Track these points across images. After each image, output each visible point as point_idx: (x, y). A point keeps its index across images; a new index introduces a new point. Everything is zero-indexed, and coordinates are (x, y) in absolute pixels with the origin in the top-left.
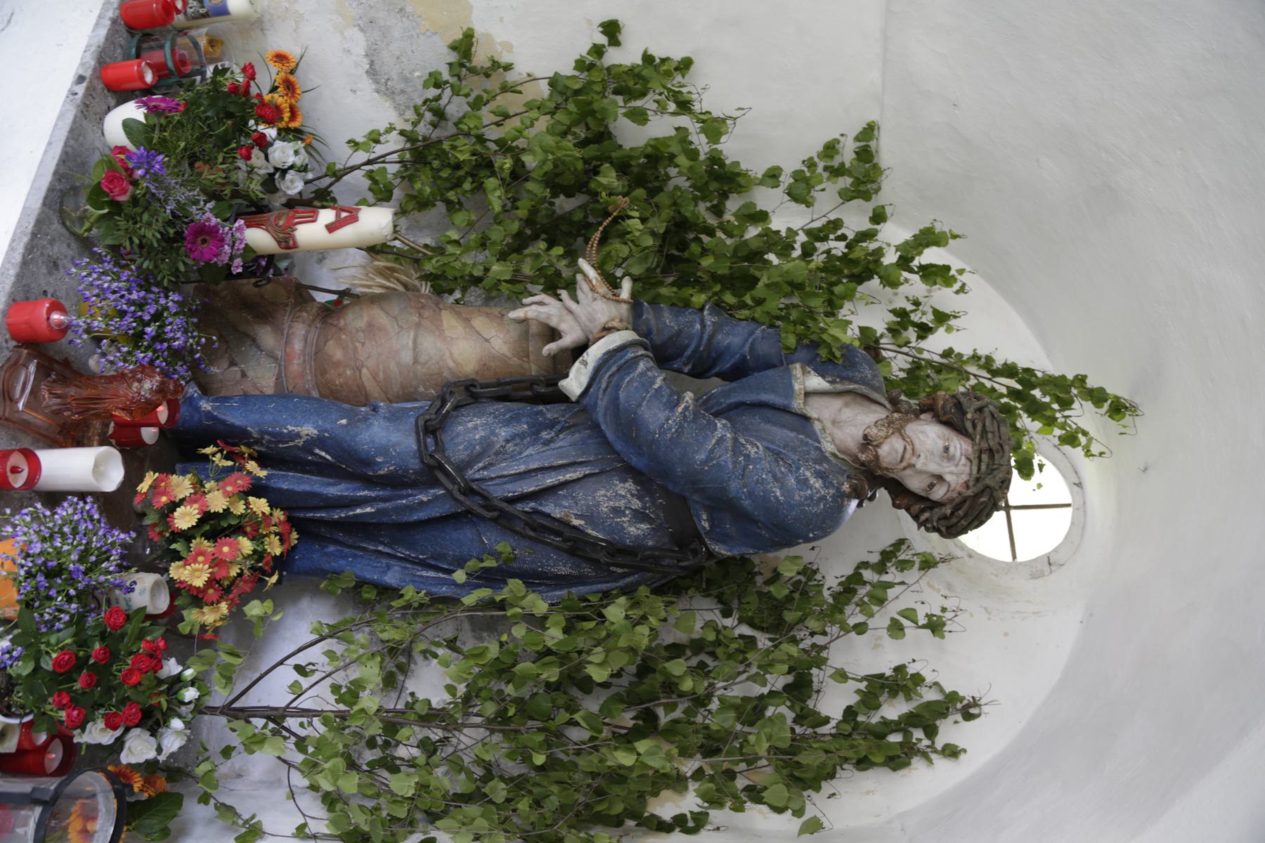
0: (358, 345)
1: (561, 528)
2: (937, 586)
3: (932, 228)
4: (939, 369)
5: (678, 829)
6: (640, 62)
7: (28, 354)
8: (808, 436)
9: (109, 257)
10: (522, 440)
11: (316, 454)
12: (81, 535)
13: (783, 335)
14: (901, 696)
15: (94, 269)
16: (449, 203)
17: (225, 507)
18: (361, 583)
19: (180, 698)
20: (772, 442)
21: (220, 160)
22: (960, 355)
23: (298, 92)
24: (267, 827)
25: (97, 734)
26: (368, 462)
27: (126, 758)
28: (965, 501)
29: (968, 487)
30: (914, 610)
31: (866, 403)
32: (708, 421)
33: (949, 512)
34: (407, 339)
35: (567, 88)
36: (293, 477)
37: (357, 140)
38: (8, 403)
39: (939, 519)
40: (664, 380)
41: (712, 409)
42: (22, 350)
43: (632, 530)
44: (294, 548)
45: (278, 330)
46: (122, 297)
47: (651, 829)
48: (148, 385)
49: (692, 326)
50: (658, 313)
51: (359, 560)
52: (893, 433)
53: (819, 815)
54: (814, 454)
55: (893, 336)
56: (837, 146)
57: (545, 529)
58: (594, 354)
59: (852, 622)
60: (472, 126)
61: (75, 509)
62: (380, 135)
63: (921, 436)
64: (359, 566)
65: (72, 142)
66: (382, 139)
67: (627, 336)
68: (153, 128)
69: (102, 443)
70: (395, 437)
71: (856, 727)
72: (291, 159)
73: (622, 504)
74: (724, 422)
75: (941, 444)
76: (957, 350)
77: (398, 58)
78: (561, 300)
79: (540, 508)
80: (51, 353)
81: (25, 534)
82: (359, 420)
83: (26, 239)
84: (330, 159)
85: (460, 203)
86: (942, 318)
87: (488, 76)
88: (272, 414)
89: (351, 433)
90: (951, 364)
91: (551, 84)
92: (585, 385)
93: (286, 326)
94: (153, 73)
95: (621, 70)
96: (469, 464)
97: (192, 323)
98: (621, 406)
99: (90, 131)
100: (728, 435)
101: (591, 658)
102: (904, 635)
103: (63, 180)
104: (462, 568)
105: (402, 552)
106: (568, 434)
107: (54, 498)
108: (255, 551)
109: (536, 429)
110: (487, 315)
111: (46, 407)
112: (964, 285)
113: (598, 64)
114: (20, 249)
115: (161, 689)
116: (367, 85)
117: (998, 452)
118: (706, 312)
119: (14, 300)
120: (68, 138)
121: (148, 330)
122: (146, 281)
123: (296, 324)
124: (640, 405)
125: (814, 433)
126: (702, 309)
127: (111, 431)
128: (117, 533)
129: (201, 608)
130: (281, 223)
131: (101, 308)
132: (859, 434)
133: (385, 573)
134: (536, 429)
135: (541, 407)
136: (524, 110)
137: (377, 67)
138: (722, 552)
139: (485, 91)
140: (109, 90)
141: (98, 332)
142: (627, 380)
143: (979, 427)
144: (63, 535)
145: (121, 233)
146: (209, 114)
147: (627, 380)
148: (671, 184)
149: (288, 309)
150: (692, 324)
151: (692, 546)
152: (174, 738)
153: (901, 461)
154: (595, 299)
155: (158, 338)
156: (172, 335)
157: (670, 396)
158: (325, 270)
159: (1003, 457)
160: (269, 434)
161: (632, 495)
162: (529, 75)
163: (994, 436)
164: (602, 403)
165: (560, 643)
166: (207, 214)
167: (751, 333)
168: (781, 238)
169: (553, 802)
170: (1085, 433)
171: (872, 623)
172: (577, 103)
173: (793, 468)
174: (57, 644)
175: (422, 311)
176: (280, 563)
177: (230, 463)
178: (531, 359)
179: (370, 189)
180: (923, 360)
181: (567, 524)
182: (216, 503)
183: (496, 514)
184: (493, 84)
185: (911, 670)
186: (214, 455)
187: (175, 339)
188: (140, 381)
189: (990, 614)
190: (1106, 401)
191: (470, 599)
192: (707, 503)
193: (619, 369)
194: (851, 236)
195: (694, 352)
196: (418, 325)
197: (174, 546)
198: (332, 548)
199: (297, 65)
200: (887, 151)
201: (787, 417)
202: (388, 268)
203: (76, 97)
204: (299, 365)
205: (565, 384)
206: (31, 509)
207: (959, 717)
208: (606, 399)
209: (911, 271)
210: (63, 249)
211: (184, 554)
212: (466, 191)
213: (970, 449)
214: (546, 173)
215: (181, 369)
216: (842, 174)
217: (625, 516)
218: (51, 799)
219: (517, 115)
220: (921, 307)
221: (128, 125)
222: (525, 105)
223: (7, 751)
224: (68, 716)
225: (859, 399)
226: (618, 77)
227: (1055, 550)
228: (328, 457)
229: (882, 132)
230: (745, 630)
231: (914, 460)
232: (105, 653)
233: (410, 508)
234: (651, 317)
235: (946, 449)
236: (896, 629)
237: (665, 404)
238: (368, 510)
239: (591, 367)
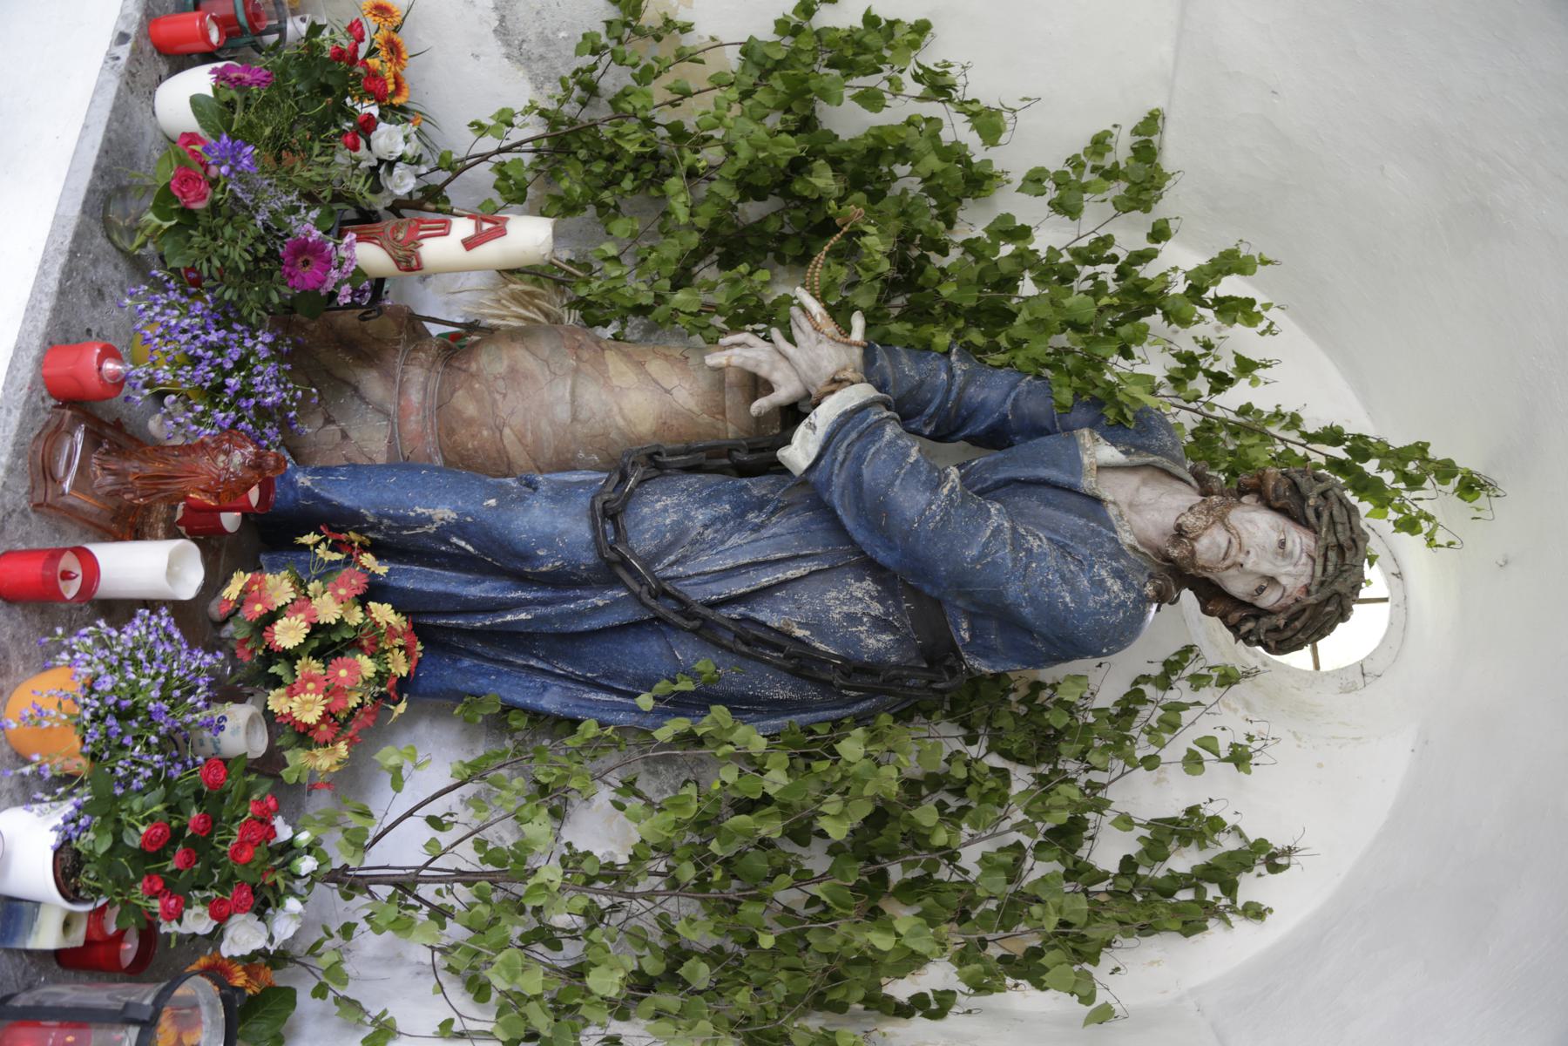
0: (498, 397)
3: (1236, 251)
4: (1236, 431)
5: (919, 1013)
6: (859, 25)
7: (73, 416)
8: (1100, 523)
9: (172, 282)
10: (724, 525)
11: (451, 544)
12: (158, 662)
13: (1055, 389)
15: (156, 299)
16: (602, 207)
18: (508, 708)
19: (294, 871)
22: (1260, 412)
24: (401, 1025)
25: (197, 921)
26: (528, 556)
27: (227, 949)
28: (1304, 610)
29: (1308, 592)
30: (1214, 739)
31: (1167, 480)
33: (1282, 623)
34: (563, 390)
36: (419, 572)
37: (483, 122)
38: (50, 484)
39: (1267, 631)
40: (920, 450)
41: (985, 490)
42: (62, 411)
43: (872, 642)
44: (419, 660)
45: (388, 376)
46: (195, 337)
47: (888, 1014)
49: (936, 376)
50: (893, 357)
51: (505, 678)
52: (1214, 523)
53: (1112, 1001)
54: (1108, 547)
55: (1176, 387)
56: (1108, 141)
58: (826, 414)
59: (1139, 755)
60: (638, 106)
61: (148, 626)
62: (514, 115)
64: (505, 686)
65: (116, 125)
66: (516, 121)
67: (858, 393)
68: (230, 105)
69: (172, 534)
70: (563, 523)
72: (400, 148)
73: (858, 609)
74: (998, 506)
75: (1275, 537)
76: (1256, 406)
77: (538, 13)
78: (771, 341)
79: (752, 615)
80: (99, 413)
81: (89, 664)
82: (513, 501)
83: (62, 260)
86: (1246, 366)
87: (658, 39)
88: (393, 491)
90: (1250, 423)
92: (813, 456)
93: (398, 370)
94: (220, 30)
95: (838, 35)
96: (657, 556)
97: (285, 370)
98: (865, 486)
100: (1006, 524)
101: (824, 809)
103: (107, 178)
105: (561, 668)
106: (782, 517)
107: (120, 610)
109: (741, 510)
110: (666, 357)
111: (100, 487)
112: (1272, 323)
113: (806, 26)
114: (56, 273)
115: (276, 863)
116: (494, 48)
117: (1349, 549)
118: (953, 358)
119: (50, 343)
120: (110, 119)
121: (231, 381)
122: (225, 316)
124: (891, 484)
125: (1108, 519)
126: (947, 353)
127: (179, 515)
128: (200, 655)
129: (310, 749)
130: (401, 236)
131: (167, 353)
132: (1169, 521)
133: (540, 695)
134: (741, 510)
135: (745, 481)
136: (708, 86)
137: (509, 24)
140: (160, 52)
141: (164, 385)
142: (872, 450)
143: (1325, 517)
144: (137, 664)
145: (195, 252)
146: (300, 88)
147: (872, 450)
148: (896, 188)
149: (400, 347)
150: (935, 373)
151: (948, 663)
152: (286, 924)
153: (1224, 559)
154: (820, 342)
155: (243, 393)
156: (262, 388)
157: (930, 472)
158: (429, 290)
159: (1356, 554)
160: (390, 517)
161: (872, 598)
162: (713, 39)
163: (1344, 530)
164: (839, 480)
165: (785, 790)
166: (306, 225)
167: (1013, 386)
168: (1039, 260)
169: (780, 990)
170: (1429, 518)
171: (1164, 755)
172: (784, 78)
174: (142, 812)
175: (579, 352)
176: (404, 685)
177: (337, 556)
178: (728, 416)
179: (495, 187)
180: (1217, 418)
181: (788, 636)
182: (325, 611)
183: (697, 623)
184: (665, 50)
185: (1209, 811)
186: (316, 545)
187: (265, 394)
188: (227, 453)
189: (1300, 739)
191: (665, 733)
193: (860, 436)
194: (1123, 258)
195: (938, 408)
196: (576, 371)
197: (273, 670)
198: (467, 663)
199: (403, 20)
200: (1171, 157)
201: (1074, 499)
202: (527, 293)
203: (119, 62)
204: (417, 422)
207: (1263, 869)
208: (843, 475)
209: (1204, 305)
210: (110, 272)
211: (287, 679)
212: (626, 192)
213: (1312, 544)
215: (271, 431)
216: (1116, 178)
217: (862, 624)
218: (152, 1018)
219: (699, 92)
220: (1213, 351)
223: (74, 945)
224: (164, 907)
225: (1157, 474)
226: (831, 45)
227: (1370, 657)
228: (469, 548)
230: (995, 761)
231: (1241, 558)
232: (205, 822)
234: (886, 363)
235: (1282, 544)
236: (1193, 762)
237: (925, 483)
238: (523, 616)
239: (821, 432)
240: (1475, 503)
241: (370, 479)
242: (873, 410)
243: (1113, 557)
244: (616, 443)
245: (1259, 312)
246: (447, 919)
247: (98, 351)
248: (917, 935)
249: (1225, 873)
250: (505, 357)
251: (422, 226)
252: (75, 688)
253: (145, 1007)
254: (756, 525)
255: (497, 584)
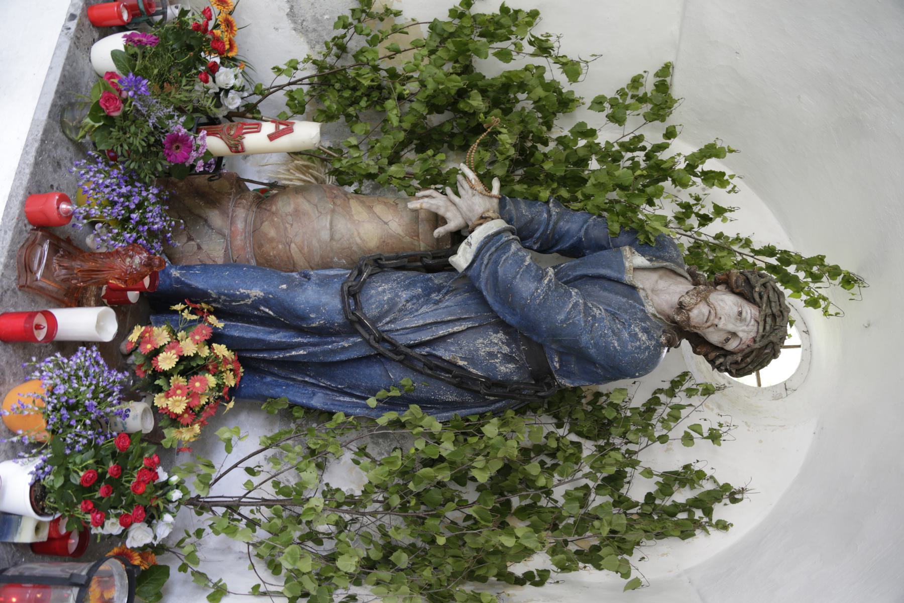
0: (288, 226)
1: (451, 368)
2: (711, 407)
3: (715, 144)
4: (713, 248)
6: (498, 12)
7: (43, 235)
8: (635, 301)
9: (100, 158)
11: (260, 311)
12: (91, 377)
13: (610, 223)
14: (687, 487)
15: (91, 168)
16: (348, 116)
17: (195, 352)
18: (292, 405)
19: (169, 498)
20: (609, 305)
21: (184, 82)
22: (728, 238)
23: (235, 28)
24: (229, 588)
25: (113, 527)
26: (304, 318)
27: (129, 544)
28: (752, 352)
29: (755, 341)
30: (700, 425)
31: (673, 276)
32: (565, 290)
33: (739, 359)
34: (326, 222)
35: (444, 31)
36: (242, 327)
38: (29, 274)
39: (731, 364)
40: (531, 258)
43: (503, 368)
44: (242, 378)
45: (224, 213)
46: (113, 190)
47: (511, 583)
48: (138, 260)
49: (541, 215)
50: (516, 204)
52: (700, 301)
54: (640, 315)
55: (679, 223)
56: (641, 80)
57: (438, 367)
58: (477, 237)
59: (657, 435)
60: (370, 59)
61: (85, 357)
62: (298, 63)
63: (721, 303)
64: (291, 392)
65: (68, 67)
66: (299, 67)
67: (496, 225)
68: (134, 56)
69: (99, 303)
70: (325, 299)
71: (655, 508)
72: (232, 82)
75: (736, 310)
76: (725, 234)
77: (312, 4)
78: (446, 194)
79: (434, 352)
80: (58, 233)
81: (51, 378)
82: (296, 286)
83: (37, 145)
84: (257, 82)
85: (357, 117)
86: (719, 211)
87: (382, 20)
89: (291, 295)
90: (722, 244)
91: (431, 28)
92: (470, 261)
93: (230, 210)
95: (486, 18)
96: (379, 318)
97: (165, 210)
98: (499, 278)
99: (80, 58)
100: (581, 301)
101: (474, 464)
102: (693, 443)
103: (63, 98)
104: (374, 396)
107: (69, 347)
108: (217, 384)
109: (428, 292)
110: (385, 204)
111: (58, 276)
112: (735, 186)
113: (467, 13)
117: (779, 317)
118: (551, 205)
119: (29, 193)
120: (65, 64)
121: (134, 216)
122: (130, 178)
123: (238, 209)
124: (515, 278)
125: (639, 299)
126: (547, 202)
127: (103, 293)
128: (115, 373)
129: (178, 428)
130: (232, 132)
131: (97, 199)
132: (675, 300)
133: (311, 398)
134: (428, 292)
135: (430, 275)
137: (295, 10)
138: (567, 384)
139: (380, 31)
140: (94, 26)
141: (95, 217)
142: (504, 258)
143: (765, 298)
144: (79, 378)
146: (174, 46)
147: (504, 258)
149: (232, 197)
151: (547, 381)
153: (706, 322)
154: (474, 195)
155: (141, 222)
156: (152, 220)
157: (537, 271)
158: (248, 164)
159: (783, 319)
160: (225, 295)
161: (503, 343)
162: (413, 20)
165: (453, 453)
166: (178, 126)
167: (586, 222)
168: (601, 149)
169: (449, 569)
170: (825, 299)
172: (454, 43)
173: (626, 325)
174: (81, 464)
175: (335, 200)
177: (194, 317)
179: (287, 105)
180: (702, 241)
182: (187, 349)
183: (402, 357)
184: (385, 26)
185: (696, 467)
186: (183, 311)
187: (153, 223)
188: (131, 257)
189: (749, 426)
190: (839, 275)
191: (383, 420)
192: (561, 350)
193: (497, 249)
194: (649, 148)
195: (542, 234)
197: (157, 382)
198: (269, 379)
199: (235, 8)
200: (677, 89)
201: (619, 286)
204: (241, 240)
205: (453, 260)
206: (53, 358)
207: (727, 501)
208: (487, 272)
209: (696, 175)
210: (64, 152)
211: (165, 388)
212: (362, 108)
213: (757, 314)
214: (428, 96)
216: (646, 102)
217: (497, 358)
219: (405, 51)
220: (700, 202)
221: (115, 55)
222: (412, 43)
223: (41, 540)
225: (668, 273)
226: (482, 24)
227: (790, 379)
228: (271, 313)
229: (676, 70)
230: (573, 437)
232: (118, 470)
233: (334, 352)
234: (512, 208)
235: (740, 313)
236: (687, 439)
237: (534, 277)
238: (301, 352)
239: (474, 247)
240: (852, 291)
241: (213, 273)
242: (504, 235)
243: (642, 320)
244: (356, 252)
245: (727, 180)
246: (257, 527)
247: (57, 197)
248: (528, 538)
249: (705, 503)
250: (292, 203)
251: (245, 127)
252: (43, 392)
253: (84, 576)
254: (437, 300)
255: (286, 334)
